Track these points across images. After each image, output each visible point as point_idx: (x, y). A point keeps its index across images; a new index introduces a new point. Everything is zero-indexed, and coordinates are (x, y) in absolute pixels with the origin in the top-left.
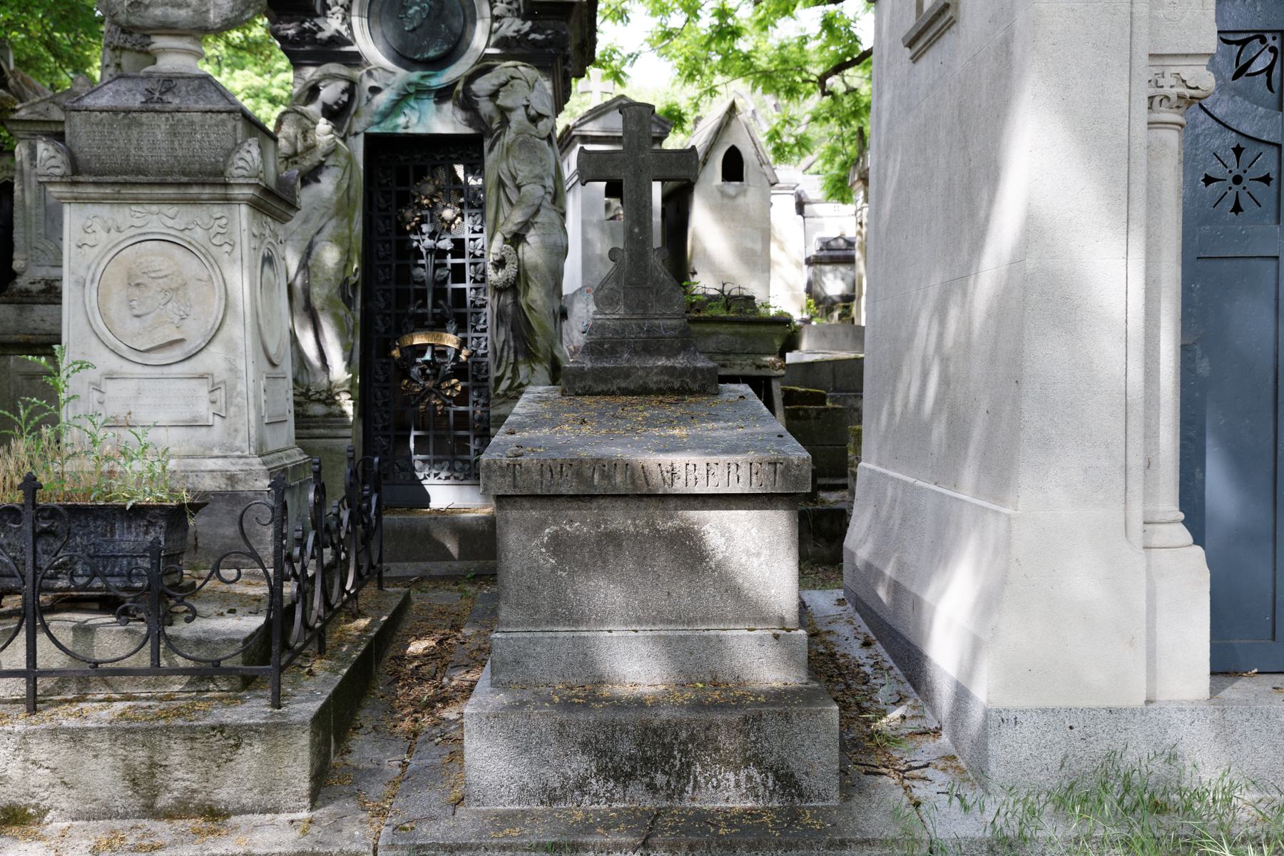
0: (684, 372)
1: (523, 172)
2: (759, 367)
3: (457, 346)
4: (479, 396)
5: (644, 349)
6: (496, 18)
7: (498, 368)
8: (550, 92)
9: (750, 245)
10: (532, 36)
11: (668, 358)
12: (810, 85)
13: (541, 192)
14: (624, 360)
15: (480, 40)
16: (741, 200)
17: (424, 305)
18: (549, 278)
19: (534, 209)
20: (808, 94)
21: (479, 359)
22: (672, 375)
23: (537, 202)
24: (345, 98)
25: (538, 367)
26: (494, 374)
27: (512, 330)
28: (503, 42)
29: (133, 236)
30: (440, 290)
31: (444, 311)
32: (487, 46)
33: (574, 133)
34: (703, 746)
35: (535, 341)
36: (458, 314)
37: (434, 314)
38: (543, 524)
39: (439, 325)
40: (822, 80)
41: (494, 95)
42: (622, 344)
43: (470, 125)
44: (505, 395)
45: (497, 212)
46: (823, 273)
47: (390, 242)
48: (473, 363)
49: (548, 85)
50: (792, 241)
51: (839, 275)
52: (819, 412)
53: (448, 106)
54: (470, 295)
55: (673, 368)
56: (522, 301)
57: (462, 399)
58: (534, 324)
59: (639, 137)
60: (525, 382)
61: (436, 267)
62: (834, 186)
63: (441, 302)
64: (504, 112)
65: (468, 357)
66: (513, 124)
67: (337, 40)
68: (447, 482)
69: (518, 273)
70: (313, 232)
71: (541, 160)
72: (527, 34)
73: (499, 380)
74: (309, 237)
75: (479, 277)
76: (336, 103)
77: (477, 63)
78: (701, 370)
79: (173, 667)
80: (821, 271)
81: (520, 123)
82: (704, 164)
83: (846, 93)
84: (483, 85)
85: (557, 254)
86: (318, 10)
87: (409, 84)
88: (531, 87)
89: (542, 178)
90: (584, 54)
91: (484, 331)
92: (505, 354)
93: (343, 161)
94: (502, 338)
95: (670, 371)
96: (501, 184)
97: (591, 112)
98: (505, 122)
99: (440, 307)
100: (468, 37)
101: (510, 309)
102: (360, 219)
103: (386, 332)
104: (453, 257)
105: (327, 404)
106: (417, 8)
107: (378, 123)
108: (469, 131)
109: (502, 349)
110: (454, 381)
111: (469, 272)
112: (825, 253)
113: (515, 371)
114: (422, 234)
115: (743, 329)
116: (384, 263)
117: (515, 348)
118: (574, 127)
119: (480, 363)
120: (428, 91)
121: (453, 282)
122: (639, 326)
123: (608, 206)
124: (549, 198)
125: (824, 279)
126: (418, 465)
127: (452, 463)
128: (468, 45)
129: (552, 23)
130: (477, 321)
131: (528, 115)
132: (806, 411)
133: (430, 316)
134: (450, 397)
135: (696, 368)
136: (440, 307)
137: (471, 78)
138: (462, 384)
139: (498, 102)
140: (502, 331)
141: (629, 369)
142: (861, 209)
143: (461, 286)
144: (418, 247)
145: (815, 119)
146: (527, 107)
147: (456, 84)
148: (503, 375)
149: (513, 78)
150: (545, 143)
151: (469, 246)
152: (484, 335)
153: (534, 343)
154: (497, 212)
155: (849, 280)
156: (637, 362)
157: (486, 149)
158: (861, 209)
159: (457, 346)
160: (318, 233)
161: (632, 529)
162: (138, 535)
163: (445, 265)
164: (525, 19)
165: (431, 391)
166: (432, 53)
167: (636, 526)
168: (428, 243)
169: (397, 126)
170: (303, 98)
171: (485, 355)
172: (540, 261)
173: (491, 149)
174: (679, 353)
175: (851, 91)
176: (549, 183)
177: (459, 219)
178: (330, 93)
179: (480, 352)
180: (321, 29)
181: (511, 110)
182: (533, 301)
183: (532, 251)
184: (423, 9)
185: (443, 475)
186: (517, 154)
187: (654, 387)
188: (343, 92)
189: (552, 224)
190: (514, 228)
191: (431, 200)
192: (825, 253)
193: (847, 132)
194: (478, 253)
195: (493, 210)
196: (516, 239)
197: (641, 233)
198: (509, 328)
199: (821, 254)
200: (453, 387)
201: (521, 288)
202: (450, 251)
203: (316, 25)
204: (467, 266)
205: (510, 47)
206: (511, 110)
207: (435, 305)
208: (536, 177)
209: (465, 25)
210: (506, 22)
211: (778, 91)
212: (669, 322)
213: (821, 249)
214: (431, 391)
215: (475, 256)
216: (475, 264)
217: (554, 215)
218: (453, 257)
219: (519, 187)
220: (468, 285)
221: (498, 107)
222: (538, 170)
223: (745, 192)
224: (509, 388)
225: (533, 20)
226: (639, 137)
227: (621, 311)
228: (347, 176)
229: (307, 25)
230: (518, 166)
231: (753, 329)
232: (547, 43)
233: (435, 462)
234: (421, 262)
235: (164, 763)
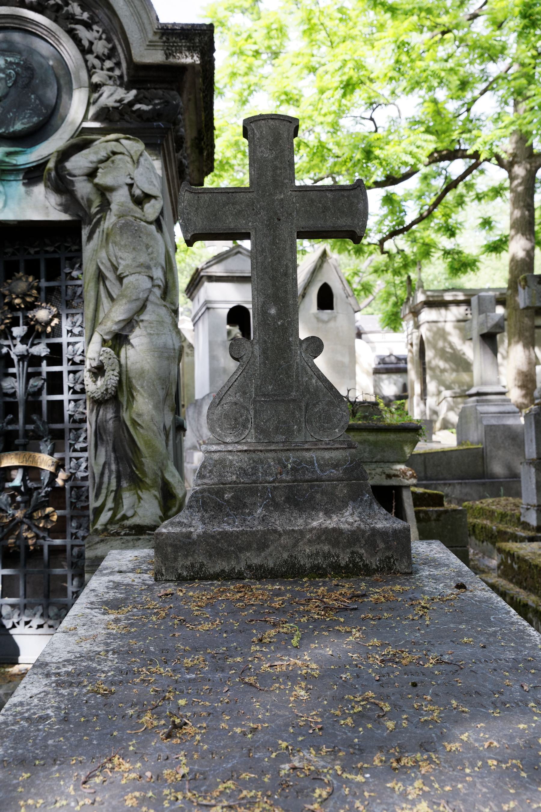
0: (354, 537)
1: (126, 260)
2: (389, 476)
3: (52, 469)
4: (79, 527)
5: (288, 500)
6: (95, 88)
7: (97, 496)
8: (159, 172)
9: (340, 358)
10: (137, 106)
12: (372, 247)
13: (148, 284)
14: (256, 520)
15: (77, 110)
16: (332, 324)
17: (15, 421)
18: (159, 387)
19: (139, 304)
20: (371, 253)
21: (80, 483)
22: (335, 544)
23: (143, 296)
25: (145, 495)
26: (93, 504)
27: (114, 450)
28: (104, 114)
30: (33, 403)
31: (38, 427)
32: (85, 119)
33: (202, 274)
35: (142, 464)
36: (53, 428)
37: (26, 432)
39: (28, 443)
40: (382, 242)
41: (92, 174)
42: (253, 492)
43: (66, 209)
44: (105, 529)
45: (96, 310)
46: (381, 380)
48: (72, 488)
49: (158, 164)
50: (367, 355)
51: (392, 381)
52: (439, 514)
53: (40, 190)
54: (69, 408)
55: (337, 531)
56: (125, 416)
57: (59, 529)
58: (140, 443)
59: (275, 168)
60: (129, 514)
61: (29, 376)
62: (390, 318)
64: (104, 191)
65: (65, 481)
66: (113, 206)
68: (40, 631)
69: (120, 382)
71: (147, 247)
72: (131, 104)
73: (98, 511)
75: (78, 387)
78: (383, 534)
80: (379, 378)
81: (122, 205)
82: (304, 296)
83: (398, 253)
84: (78, 163)
85: (168, 358)
88: (136, 163)
89: (149, 268)
90: (201, 153)
91: (84, 450)
92: (106, 479)
94: (102, 460)
95: (333, 536)
96: (101, 277)
97: (215, 257)
98: (105, 205)
100: (61, 110)
101: (111, 425)
104: (48, 365)
108: (65, 217)
109: (102, 474)
110: (49, 510)
111: (67, 381)
112: (382, 366)
113: (118, 500)
114: (14, 338)
115: (372, 437)
117: (118, 472)
118: (202, 269)
119: (79, 488)
120: (15, 170)
121: (49, 393)
122: (279, 461)
123: (229, 333)
124: (158, 292)
125: (382, 384)
126: (5, 611)
127: (46, 608)
128: (63, 119)
129: (160, 92)
130: (77, 439)
131: (132, 196)
132: (426, 512)
133: (21, 433)
134: (44, 529)
135: (373, 529)
136: (33, 422)
137: (65, 154)
138: (59, 512)
139: (96, 180)
140: (102, 451)
141: (265, 533)
142: (412, 334)
144: (8, 354)
145: (376, 271)
146: (131, 186)
147: (47, 162)
148: (103, 505)
149: (114, 153)
150: (153, 228)
151: (67, 353)
152: (86, 454)
153: (140, 466)
154: (96, 310)
155: (400, 385)
156: (279, 522)
157: (84, 237)
158: (412, 334)
159: (52, 469)
163: (40, 374)
165: (22, 522)
166: (18, 126)
168: (21, 348)
171: (85, 479)
172: (147, 367)
173: (90, 238)
174: (345, 506)
175: (400, 252)
176: (158, 274)
177: (56, 321)
179: (80, 474)
181: (111, 189)
182: (139, 415)
183: (138, 352)
184: (9, 76)
185: (36, 621)
186: (118, 238)
187: (307, 563)
189: (161, 323)
190: (115, 328)
191: (23, 299)
192: (382, 366)
193: (397, 280)
194: (77, 359)
195: (92, 306)
196: (118, 340)
198: (110, 448)
199: (380, 366)
200: (47, 517)
201: (124, 400)
202: (45, 357)
204: (65, 375)
205: (113, 119)
206: (111, 189)
207: (28, 420)
208: (141, 265)
209: (59, 96)
210: (106, 91)
211: (349, 251)
212: (327, 455)
213: (379, 364)
214: (22, 522)
215: (74, 363)
216: (75, 372)
217: (163, 312)
218: (48, 365)
219: (120, 279)
220: (66, 396)
221: (97, 186)
222: (143, 258)
223: (335, 318)
224: (111, 521)
225: (138, 89)
226: (275, 168)
227: (251, 438)
230: (120, 254)
231: (381, 437)
232: (156, 115)
233: (25, 607)
234: (11, 370)
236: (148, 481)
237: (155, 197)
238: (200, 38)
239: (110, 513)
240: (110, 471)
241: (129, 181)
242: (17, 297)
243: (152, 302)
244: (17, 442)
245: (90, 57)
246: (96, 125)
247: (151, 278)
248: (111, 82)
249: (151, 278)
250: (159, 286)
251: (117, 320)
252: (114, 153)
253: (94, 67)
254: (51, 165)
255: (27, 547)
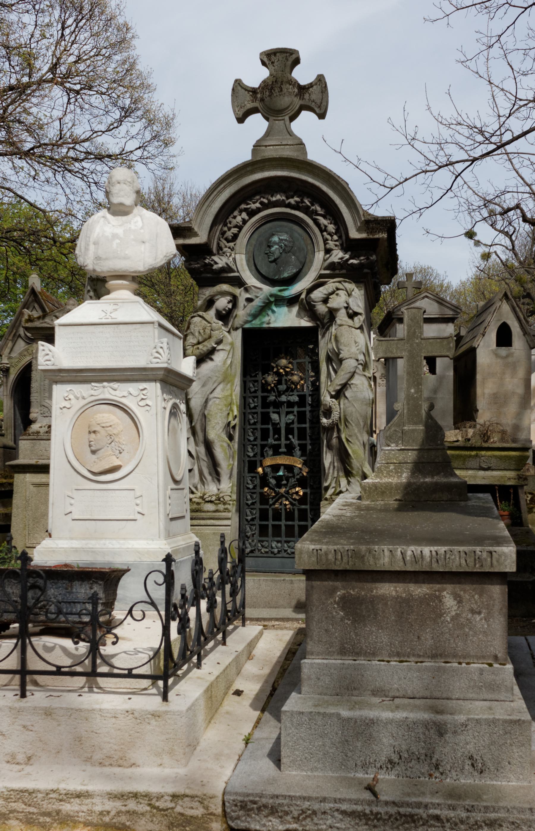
6: (328, 251)
10: (351, 261)
11: (433, 477)
19: (350, 375)
23: (352, 370)
24: (230, 306)
29: (92, 402)
34: (519, 725)
38: (334, 590)
41: (325, 301)
47: (257, 397)
63: (291, 437)
67: (228, 269)
70: (208, 393)
72: (348, 260)
74: (206, 397)
76: (224, 310)
77: (314, 280)
79: (227, 633)
84: (318, 294)
85: (366, 405)
86: (215, 251)
87: (271, 295)
93: (228, 348)
99: (289, 439)
102: (239, 383)
103: (255, 456)
105: (216, 504)
106: (277, 247)
107: (251, 321)
116: (254, 411)
137: (310, 290)
139: (328, 305)
143: (304, 426)
146: (346, 308)
147: (301, 294)
149: (338, 289)
160: (211, 393)
161: (394, 593)
162: (86, 590)
164: (346, 252)
167: (397, 591)
169: (263, 323)
170: (204, 307)
173: (323, 336)
178: (222, 303)
180: (216, 263)
188: (229, 303)
197: (416, 392)
200: (297, 493)
203: (213, 260)
210: (334, 252)
218: (298, 407)
228: (230, 356)
229: (207, 261)
235: (98, 732)
236: (354, 472)
237: (361, 314)
238: (389, 225)
239: (333, 489)
240: (334, 467)
241: (346, 305)
242: (281, 368)
243: (358, 374)
244: (280, 450)
245: (325, 233)
246: (327, 272)
247: (357, 360)
248: (337, 248)
249: (357, 360)
250: (361, 364)
251: (339, 383)
252: (338, 289)
253: (327, 240)
254: (303, 296)
255: (286, 509)
